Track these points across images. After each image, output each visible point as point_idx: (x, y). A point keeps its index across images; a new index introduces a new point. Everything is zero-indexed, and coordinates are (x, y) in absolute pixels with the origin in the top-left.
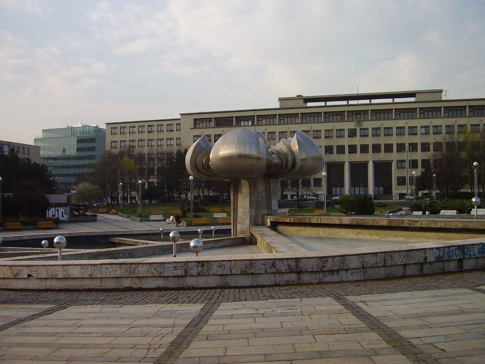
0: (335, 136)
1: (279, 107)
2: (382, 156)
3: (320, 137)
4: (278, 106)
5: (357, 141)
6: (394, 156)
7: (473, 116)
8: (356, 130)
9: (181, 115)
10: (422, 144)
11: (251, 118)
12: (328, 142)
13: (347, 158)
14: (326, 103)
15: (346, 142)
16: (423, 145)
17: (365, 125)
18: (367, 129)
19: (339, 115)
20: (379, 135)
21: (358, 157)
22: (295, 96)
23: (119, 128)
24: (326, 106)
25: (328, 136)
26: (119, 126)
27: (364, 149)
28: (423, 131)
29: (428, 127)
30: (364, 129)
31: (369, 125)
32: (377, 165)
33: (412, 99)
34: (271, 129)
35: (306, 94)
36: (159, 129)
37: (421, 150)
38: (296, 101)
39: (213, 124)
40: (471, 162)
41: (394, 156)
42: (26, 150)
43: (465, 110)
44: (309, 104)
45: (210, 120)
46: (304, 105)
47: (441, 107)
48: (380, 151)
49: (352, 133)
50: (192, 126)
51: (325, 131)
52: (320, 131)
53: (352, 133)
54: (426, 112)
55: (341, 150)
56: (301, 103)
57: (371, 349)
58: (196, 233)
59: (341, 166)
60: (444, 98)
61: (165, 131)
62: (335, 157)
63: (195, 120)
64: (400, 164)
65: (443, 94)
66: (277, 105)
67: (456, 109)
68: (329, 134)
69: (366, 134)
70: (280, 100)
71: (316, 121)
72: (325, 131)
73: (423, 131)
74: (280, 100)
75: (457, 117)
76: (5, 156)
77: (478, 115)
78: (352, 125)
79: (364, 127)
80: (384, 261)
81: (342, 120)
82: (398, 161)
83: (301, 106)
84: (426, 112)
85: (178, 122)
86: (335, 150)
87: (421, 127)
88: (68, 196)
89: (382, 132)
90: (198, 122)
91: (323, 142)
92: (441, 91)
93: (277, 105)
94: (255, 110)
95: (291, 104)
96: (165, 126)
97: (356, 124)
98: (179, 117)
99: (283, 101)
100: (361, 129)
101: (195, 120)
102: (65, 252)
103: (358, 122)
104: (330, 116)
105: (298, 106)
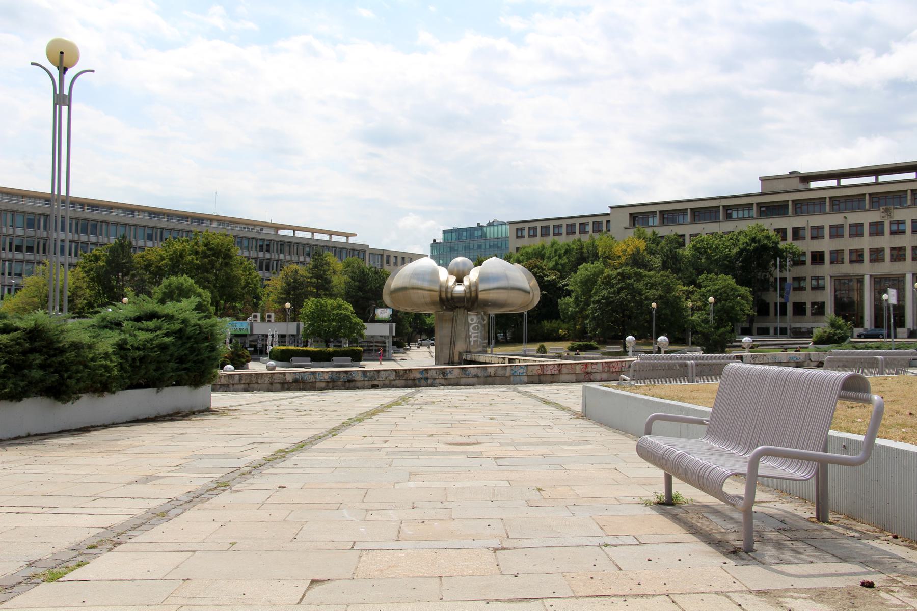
1: (760, 191)
3: (823, 237)
5: (886, 242)
8: (882, 224)
9: (612, 208)
14: (877, 179)
15: (866, 243)
17: (899, 214)
18: (903, 222)
23: (527, 229)
26: (527, 226)
36: (569, 231)
37: (900, 260)
38: (787, 180)
39: (754, 212)
41: (866, 269)
44: (814, 185)
45: (749, 206)
47: (686, 209)
49: (877, 229)
50: (627, 225)
52: (822, 227)
53: (877, 229)
56: (796, 184)
58: (173, 371)
61: (527, 236)
72: (831, 227)
74: (763, 180)
78: (875, 216)
79: (896, 218)
83: (794, 188)
85: (607, 218)
90: (799, 205)
93: (756, 187)
94: (720, 198)
95: (780, 186)
97: (883, 215)
98: (609, 211)
100: (891, 223)
102: (832, 575)
103: (887, 211)
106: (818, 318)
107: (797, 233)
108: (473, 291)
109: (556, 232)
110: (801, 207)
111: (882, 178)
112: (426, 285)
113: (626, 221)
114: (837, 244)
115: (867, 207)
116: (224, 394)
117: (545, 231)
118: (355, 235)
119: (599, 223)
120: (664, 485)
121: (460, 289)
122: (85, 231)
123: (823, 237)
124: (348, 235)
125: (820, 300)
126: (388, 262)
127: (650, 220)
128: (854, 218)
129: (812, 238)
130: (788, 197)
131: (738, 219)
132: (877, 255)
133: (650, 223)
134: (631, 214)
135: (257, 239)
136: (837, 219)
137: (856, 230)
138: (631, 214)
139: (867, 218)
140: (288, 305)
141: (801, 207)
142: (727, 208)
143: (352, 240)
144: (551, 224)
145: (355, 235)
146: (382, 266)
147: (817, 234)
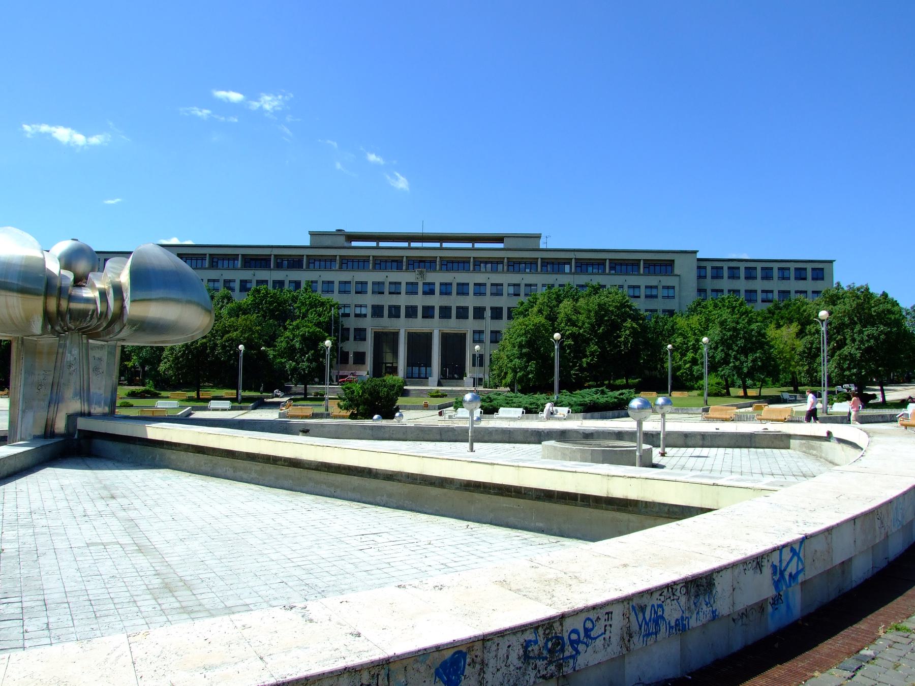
0: (488, 292)
1: (308, 244)
2: (453, 325)
3: (366, 292)
4: (307, 243)
5: (419, 301)
6: (468, 326)
7: (649, 274)
8: (417, 284)
10: (441, 308)
12: (378, 300)
13: (403, 327)
15: (403, 301)
16: (510, 310)
19: (395, 263)
20: (349, 292)
21: (419, 325)
22: (333, 229)
24: (377, 248)
25: (360, 290)
26: (792, 266)
27: (428, 312)
28: (511, 290)
29: (519, 285)
30: (429, 284)
31: (437, 278)
32: (445, 337)
33: (501, 246)
34: (228, 275)
35: (350, 229)
39: (239, 263)
41: (468, 326)
43: (604, 264)
44: (354, 244)
45: (235, 257)
46: (346, 244)
49: (412, 289)
51: (374, 283)
53: (412, 289)
54: (514, 265)
55: (394, 312)
56: (341, 241)
59: (427, 338)
60: (542, 246)
62: (386, 324)
64: (477, 336)
65: (542, 240)
67: (555, 263)
68: (378, 288)
69: (347, 289)
70: (312, 234)
71: (231, 266)
72: (374, 283)
73: (511, 290)
74: (312, 234)
75: (627, 274)
77: (553, 272)
81: (399, 268)
82: (474, 332)
84: (514, 265)
86: (386, 312)
87: (509, 285)
88: (518, 387)
89: (353, 288)
91: (370, 299)
92: (538, 237)
93: (306, 241)
94: (574, 250)
95: (328, 241)
99: (317, 237)
103: (421, 273)
104: (382, 263)
105: (336, 245)
106: (360, 366)
107: (344, 287)
110: (348, 263)
111: (477, 245)
114: (445, 301)
115: (471, 268)
116: (402, 470)
120: (18, 481)
123: (366, 292)
125: (361, 350)
128: (360, 276)
129: (357, 293)
130: (335, 252)
131: (593, 274)
132: (411, 312)
137: (395, 289)
139: (405, 277)
140: (760, 364)
141: (348, 263)
147: (395, 289)
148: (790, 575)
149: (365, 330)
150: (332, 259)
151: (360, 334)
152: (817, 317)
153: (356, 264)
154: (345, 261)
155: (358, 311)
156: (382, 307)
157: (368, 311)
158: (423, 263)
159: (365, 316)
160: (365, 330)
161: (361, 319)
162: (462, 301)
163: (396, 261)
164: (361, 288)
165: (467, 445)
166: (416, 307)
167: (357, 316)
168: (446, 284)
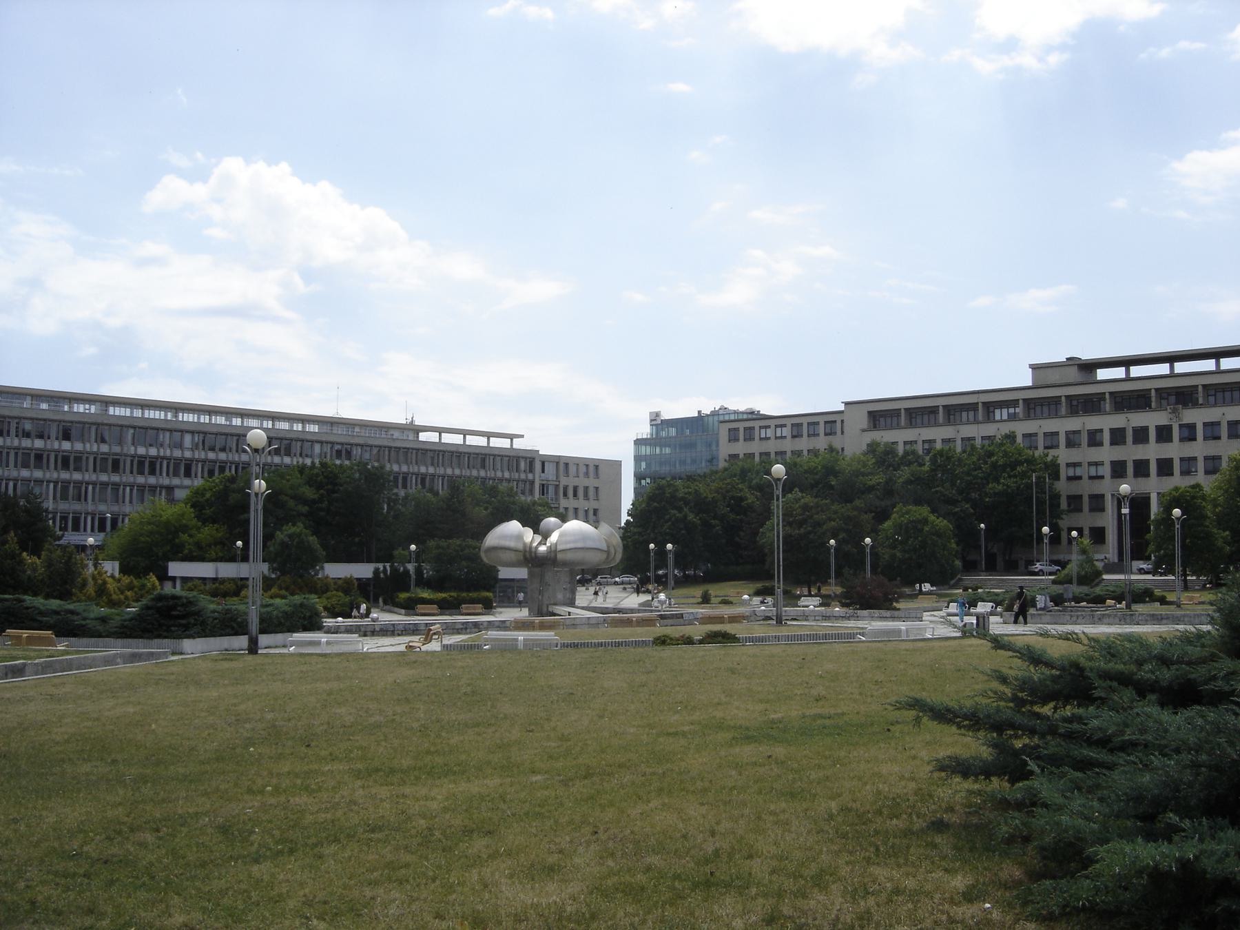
1: (1030, 384)
9: (847, 404)
11: (973, 407)
12: (1119, 453)
15: (1152, 451)
26: (789, 422)
40: (54, 770)
42: (591, 469)
48: (1147, 475)
49: (1164, 434)
52: (1057, 433)
53: (1164, 434)
56: (1073, 374)
57: (899, 706)
63: (871, 414)
66: (1026, 380)
68: (1118, 437)
70: (1035, 368)
74: (1035, 368)
76: (242, 517)
80: (418, 778)
91: (1107, 453)
93: (1026, 380)
95: (1054, 377)
96: (822, 425)
98: (842, 407)
100: (1181, 426)
101: (871, 414)
103: (1174, 411)
108: (553, 551)
109: (828, 431)
110: (1090, 404)
112: (512, 544)
113: (864, 421)
117: (990, 407)
118: (522, 436)
119: (830, 423)
121: (543, 548)
122: (26, 465)
124: (511, 437)
125: (1099, 524)
126: (565, 494)
127: (997, 412)
133: (998, 417)
134: (869, 413)
135: (333, 443)
136: (1074, 424)
137: (1141, 435)
138: (869, 413)
141: (1090, 404)
142: (909, 411)
143: (518, 444)
144: (805, 421)
145: (522, 436)
146: (557, 499)
148: (1013, 781)
149: (1103, 496)
150: (1056, 401)
151: (1097, 503)
152: (769, 473)
153: (1046, 409)
154: (1164, 395)
155: (1093, 472)
156: (1124, 462)
157: (1106, 470)
158: (1182, 395)
159: (1102, 477)
160: (1103, 496)
161: (1096, 481)
162: (1119, 453)
163: (1144, 396)
164: (1094, 439)
165: (242, 641)
166: (1148, 461)
167: (1091, 478)
168: (1030, 435)
